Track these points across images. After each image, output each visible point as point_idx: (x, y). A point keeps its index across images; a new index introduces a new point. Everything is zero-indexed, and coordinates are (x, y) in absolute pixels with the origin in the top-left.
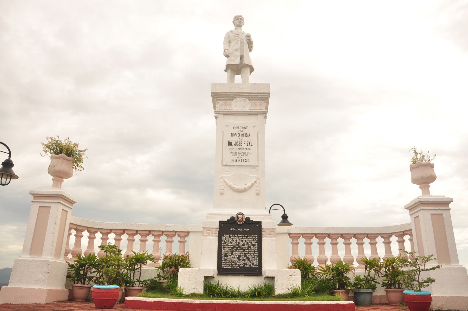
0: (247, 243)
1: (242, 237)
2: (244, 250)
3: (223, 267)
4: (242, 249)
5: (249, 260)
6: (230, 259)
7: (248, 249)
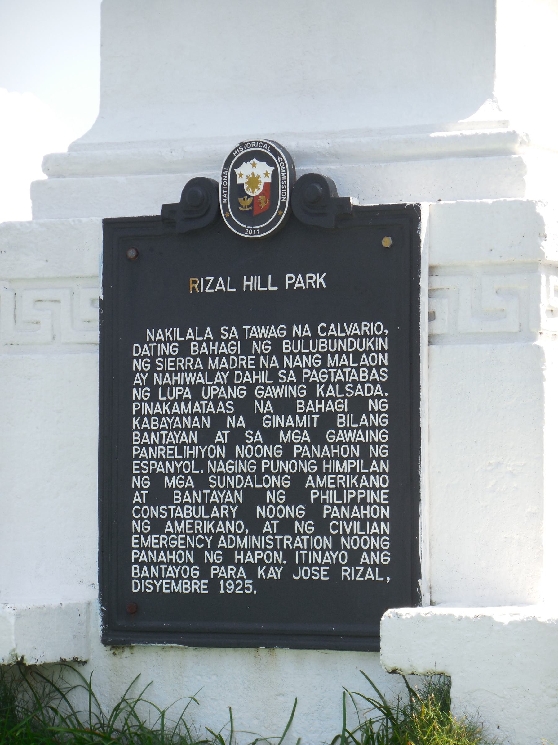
0: (311, 395)
1: (276, 343)
2: (288, 448)
3: (140, 580)
4: (271, 436)
5: (322, 528)
6: (186, 520)
7: (318, 437)
